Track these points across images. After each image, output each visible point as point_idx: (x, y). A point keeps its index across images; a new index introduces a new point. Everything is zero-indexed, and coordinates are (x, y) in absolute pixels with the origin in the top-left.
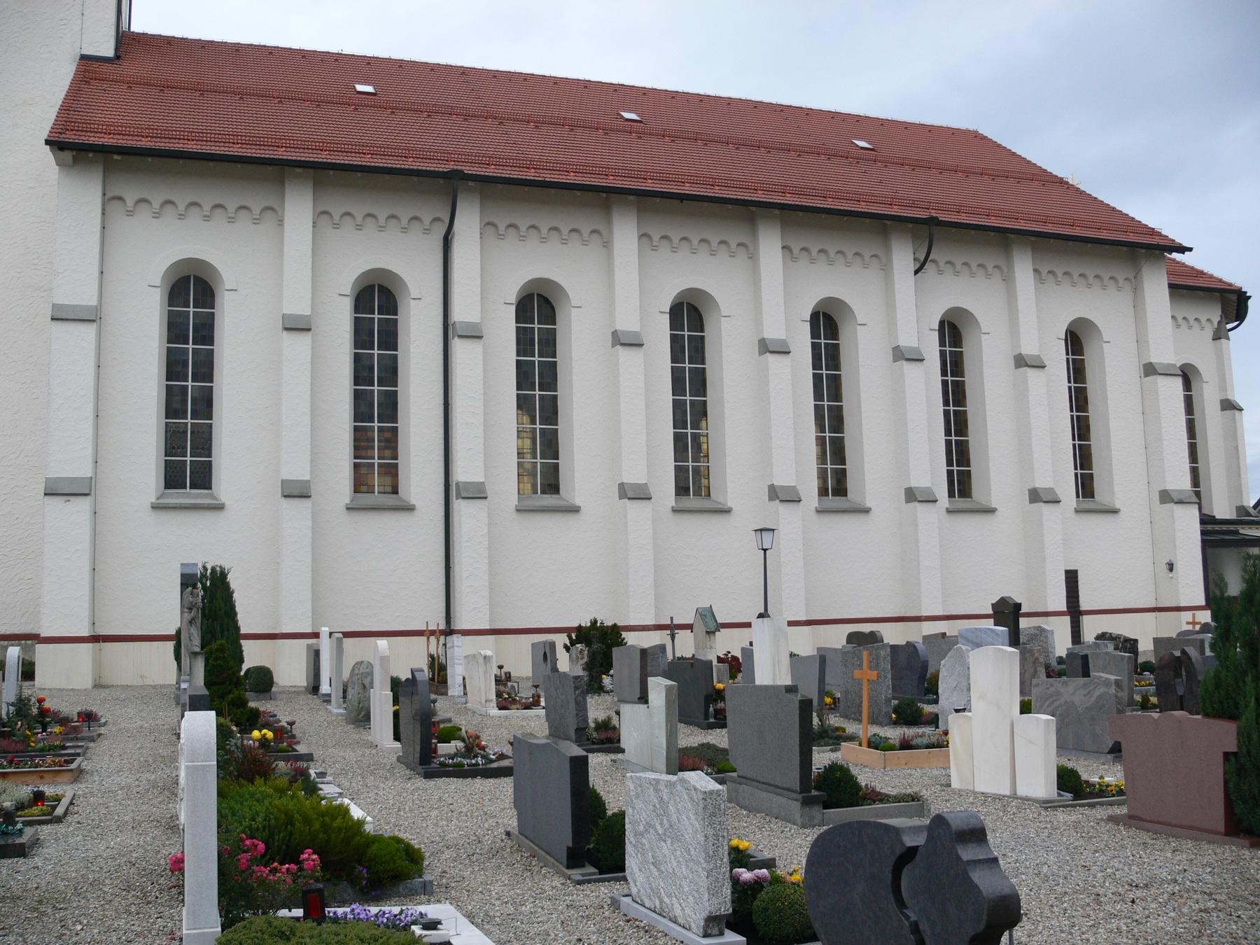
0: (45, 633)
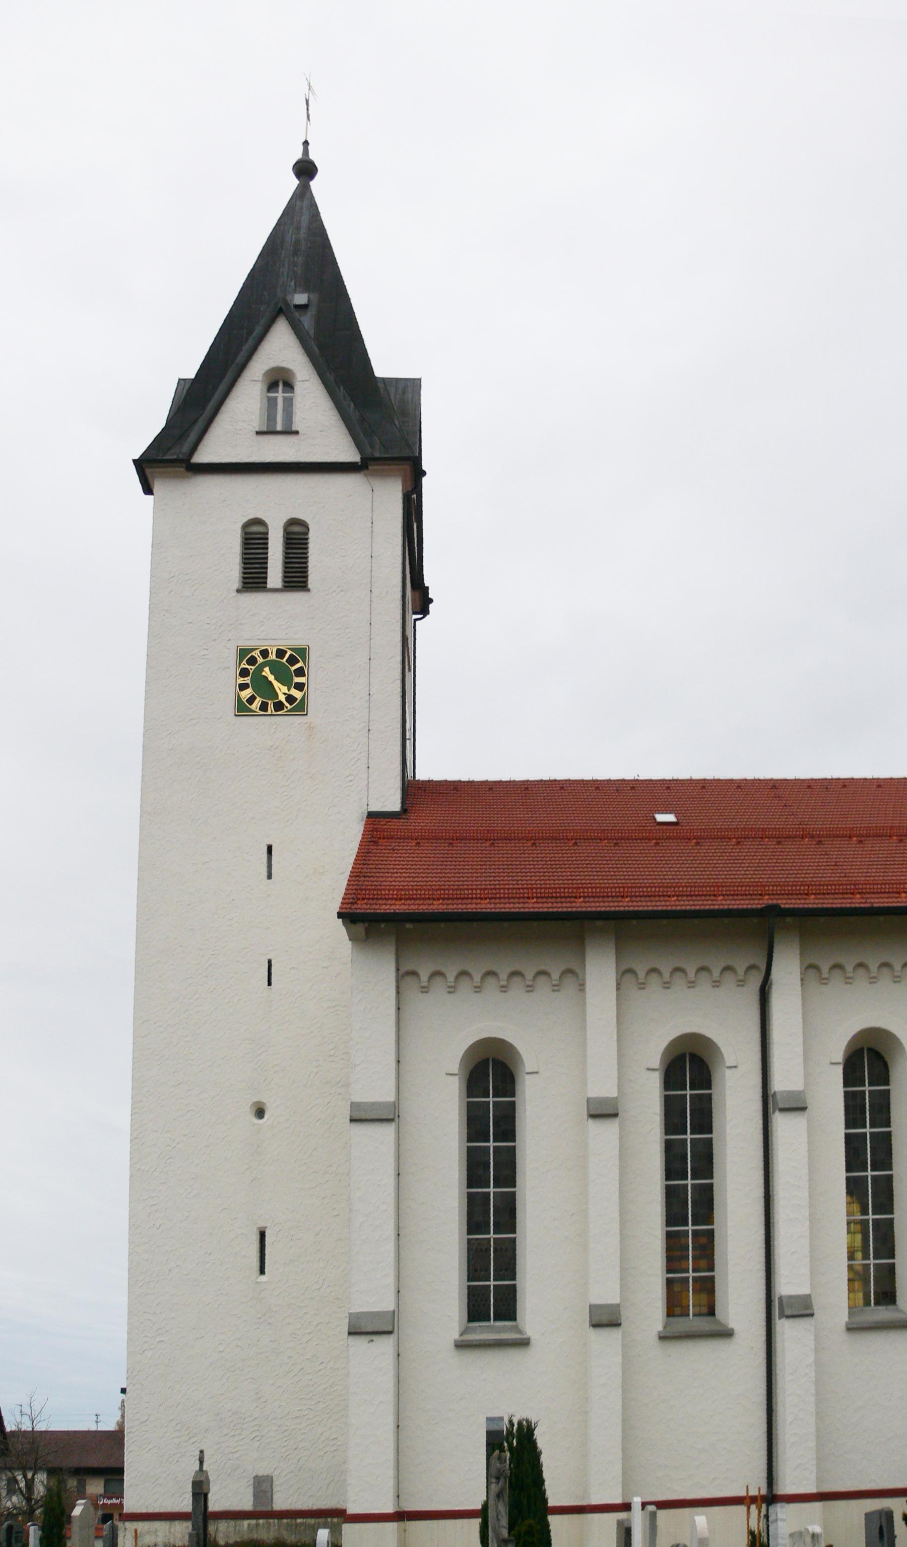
0: (352, 1510)
